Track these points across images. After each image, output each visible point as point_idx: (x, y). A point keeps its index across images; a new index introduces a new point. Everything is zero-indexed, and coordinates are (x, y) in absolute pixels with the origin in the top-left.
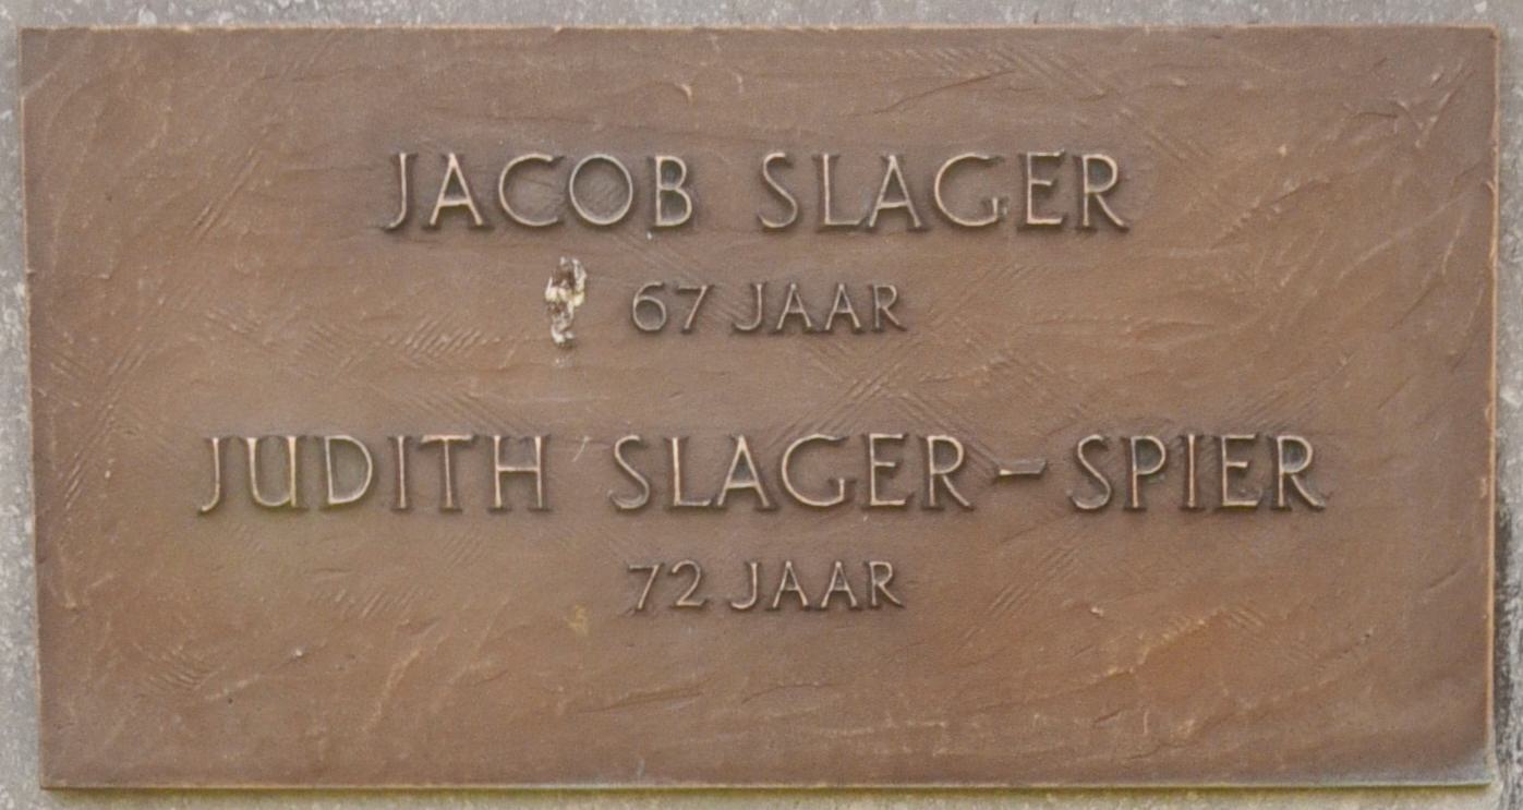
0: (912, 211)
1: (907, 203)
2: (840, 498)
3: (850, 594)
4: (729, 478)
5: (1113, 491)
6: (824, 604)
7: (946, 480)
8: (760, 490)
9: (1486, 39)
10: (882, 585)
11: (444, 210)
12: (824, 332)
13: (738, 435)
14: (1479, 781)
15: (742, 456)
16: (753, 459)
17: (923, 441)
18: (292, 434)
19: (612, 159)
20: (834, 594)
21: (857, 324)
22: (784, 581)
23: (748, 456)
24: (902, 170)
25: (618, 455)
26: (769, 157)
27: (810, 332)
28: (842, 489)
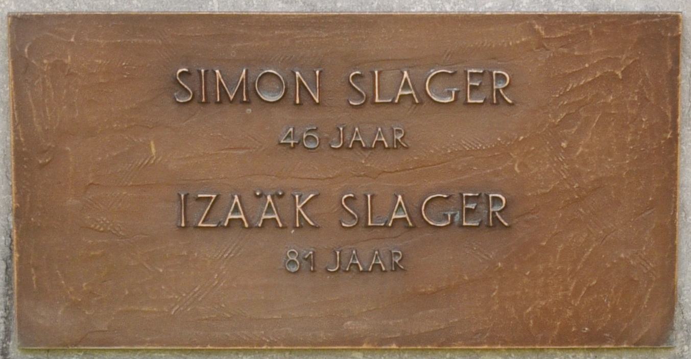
0: (414, 96)
1: (412, 92)
2: (448, 223)
3: (382, 266)
4: (230, 214)
5: (359, 218)
6: (370, 269)
7: (497, 214)
8: (244, 220)
9: (674, 19)
10: (397, 261)
11: (401, 96)
12: (371, 148)
13: (235, 195)
14: (671, 346)
15: (236, 204)
16: (405, 205)
17: (487, 197)
18: (297, 194)
19: (275, 72)
20: (374, 265)
21: (386, 146)
22: (352, 259)
23: (272, 204)
24: (410, 78)
25: (343, 203)
26: (180, 71)
27: (365, 149)
28: (449, 219)
